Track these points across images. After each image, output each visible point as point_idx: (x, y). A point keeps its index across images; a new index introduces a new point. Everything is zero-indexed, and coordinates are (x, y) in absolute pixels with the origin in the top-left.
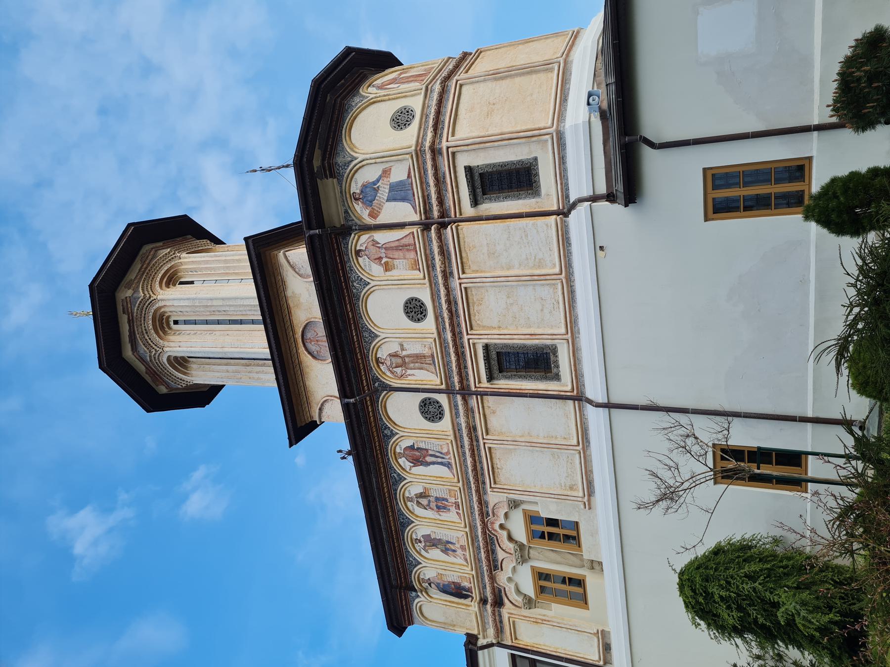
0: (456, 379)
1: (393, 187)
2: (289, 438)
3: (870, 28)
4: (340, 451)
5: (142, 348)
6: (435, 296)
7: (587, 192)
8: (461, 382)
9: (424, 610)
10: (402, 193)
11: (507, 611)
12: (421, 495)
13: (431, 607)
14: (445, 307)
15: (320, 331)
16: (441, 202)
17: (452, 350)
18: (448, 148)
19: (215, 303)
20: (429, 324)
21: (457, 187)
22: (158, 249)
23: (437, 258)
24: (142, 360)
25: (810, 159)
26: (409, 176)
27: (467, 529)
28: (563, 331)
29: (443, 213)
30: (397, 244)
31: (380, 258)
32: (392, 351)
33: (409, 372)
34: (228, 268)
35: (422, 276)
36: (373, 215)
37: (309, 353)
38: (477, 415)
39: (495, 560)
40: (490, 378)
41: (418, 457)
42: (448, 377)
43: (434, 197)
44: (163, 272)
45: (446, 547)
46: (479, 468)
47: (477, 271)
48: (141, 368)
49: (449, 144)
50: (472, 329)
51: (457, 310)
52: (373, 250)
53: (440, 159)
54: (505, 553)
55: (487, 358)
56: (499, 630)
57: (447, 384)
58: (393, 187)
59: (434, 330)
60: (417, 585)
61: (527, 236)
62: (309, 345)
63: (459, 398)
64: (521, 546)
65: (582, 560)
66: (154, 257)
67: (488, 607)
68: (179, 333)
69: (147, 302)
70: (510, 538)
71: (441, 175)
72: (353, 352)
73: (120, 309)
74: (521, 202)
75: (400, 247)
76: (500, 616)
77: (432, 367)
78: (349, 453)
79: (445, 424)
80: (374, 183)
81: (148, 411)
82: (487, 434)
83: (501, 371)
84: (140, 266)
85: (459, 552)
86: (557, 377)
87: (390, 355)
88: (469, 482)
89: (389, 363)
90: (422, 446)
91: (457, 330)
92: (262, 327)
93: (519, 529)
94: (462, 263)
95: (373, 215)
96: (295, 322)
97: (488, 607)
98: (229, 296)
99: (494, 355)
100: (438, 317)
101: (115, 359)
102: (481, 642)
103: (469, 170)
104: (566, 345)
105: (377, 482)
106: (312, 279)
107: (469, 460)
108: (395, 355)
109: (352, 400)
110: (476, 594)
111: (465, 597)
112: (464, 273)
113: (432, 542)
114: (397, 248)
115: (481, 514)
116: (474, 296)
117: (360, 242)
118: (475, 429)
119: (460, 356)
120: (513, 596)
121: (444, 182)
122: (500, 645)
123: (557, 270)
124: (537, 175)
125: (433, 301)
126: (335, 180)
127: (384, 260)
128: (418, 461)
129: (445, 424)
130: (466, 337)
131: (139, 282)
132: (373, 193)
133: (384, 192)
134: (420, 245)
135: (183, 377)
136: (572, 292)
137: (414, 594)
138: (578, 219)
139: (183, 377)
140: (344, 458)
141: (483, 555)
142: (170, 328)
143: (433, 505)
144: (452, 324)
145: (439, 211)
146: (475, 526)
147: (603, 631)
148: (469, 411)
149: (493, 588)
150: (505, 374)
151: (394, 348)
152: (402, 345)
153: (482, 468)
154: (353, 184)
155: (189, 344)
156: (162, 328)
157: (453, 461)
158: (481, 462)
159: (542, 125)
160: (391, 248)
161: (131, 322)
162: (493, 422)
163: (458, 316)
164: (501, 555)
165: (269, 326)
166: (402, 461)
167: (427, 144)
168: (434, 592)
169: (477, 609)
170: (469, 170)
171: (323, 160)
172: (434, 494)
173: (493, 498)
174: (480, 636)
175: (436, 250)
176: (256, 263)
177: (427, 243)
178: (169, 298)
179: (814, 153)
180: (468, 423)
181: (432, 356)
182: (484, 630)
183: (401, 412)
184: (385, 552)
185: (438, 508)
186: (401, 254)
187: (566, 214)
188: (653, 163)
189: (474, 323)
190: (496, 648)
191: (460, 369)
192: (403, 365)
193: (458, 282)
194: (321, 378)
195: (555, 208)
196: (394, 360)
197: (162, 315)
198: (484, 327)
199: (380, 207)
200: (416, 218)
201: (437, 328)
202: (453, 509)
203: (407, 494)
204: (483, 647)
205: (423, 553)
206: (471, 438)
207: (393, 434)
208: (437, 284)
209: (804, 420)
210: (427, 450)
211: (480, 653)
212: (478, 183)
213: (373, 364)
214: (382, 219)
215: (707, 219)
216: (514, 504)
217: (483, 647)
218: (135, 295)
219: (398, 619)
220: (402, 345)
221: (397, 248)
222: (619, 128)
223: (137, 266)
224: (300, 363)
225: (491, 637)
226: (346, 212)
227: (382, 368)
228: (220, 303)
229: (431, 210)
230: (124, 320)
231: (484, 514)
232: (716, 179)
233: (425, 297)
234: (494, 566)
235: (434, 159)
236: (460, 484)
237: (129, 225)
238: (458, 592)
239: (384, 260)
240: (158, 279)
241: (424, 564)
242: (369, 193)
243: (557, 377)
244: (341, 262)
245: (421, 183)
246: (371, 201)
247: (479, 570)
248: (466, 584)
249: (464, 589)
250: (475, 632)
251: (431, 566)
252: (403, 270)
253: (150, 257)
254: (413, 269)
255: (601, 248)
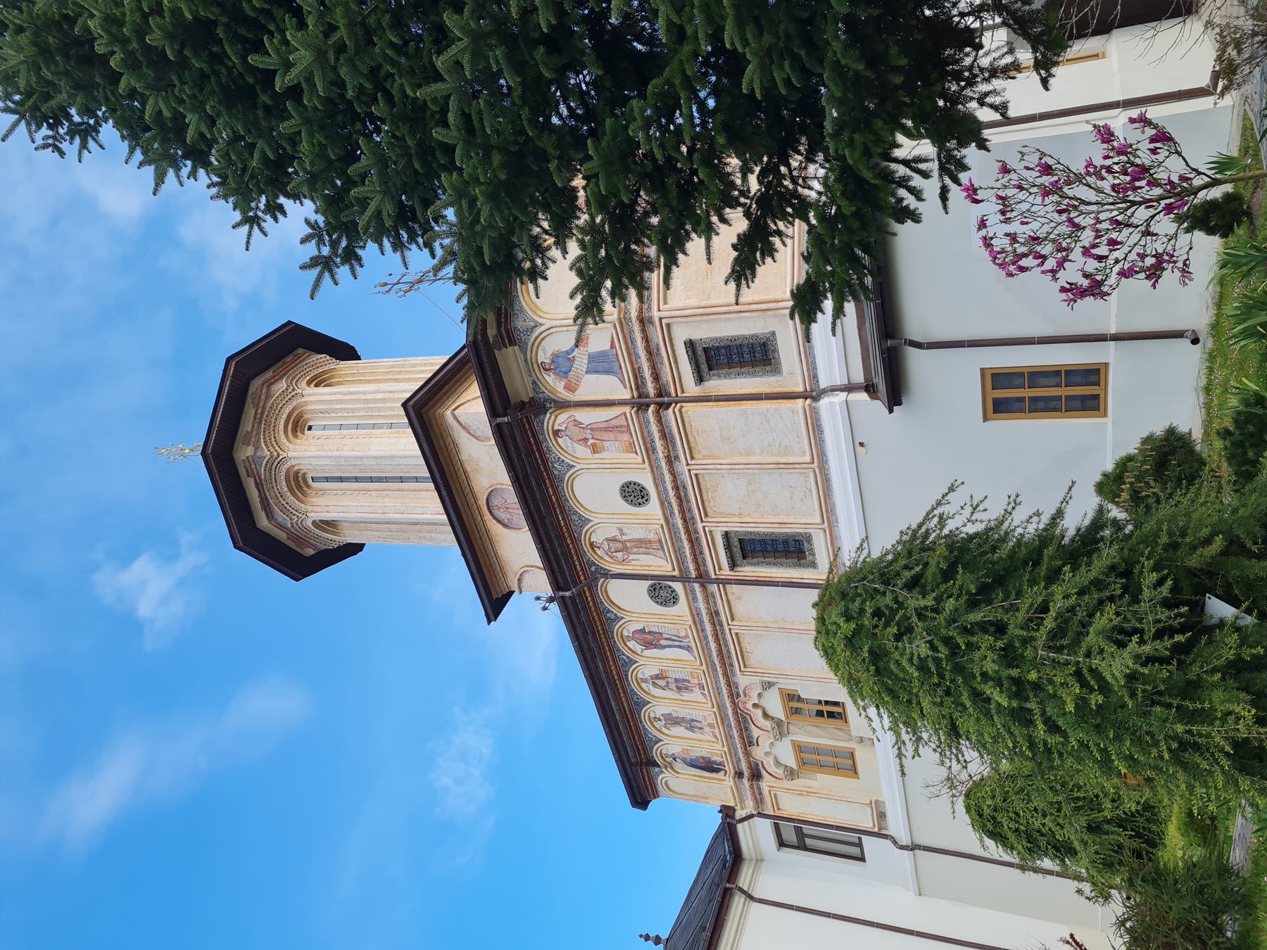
0: (691, 567)
1: (592, 358)
2: (487, 615)
3: (1159, 429)
4: (538, 598)
5: (280, 516)
6: (658, 481)
7: (840, 380)
8: (698, 568)
9: (670, 784)
10: (605, 365)
11: (766, 783)
12: (657, 677)
13: (677, 783)
14: (671, 493)
15: (510, 496)
16: (656, 377)
17: (684, 537)
18: (661, 319)
19: (366, 462)
20: (653, 508)
21: (676, 362)
22: (270, 383)
23: (659, 444)
24: (282, 527)
25: (1106, 365)
26: (612, 346)
27: (715, 709)
28: (818, 520)
29: (661, 392)
30: (605, 425)
31: (586, 440)
32: (610, 535)
33: (632, 557)
34: (370, 408)
35: (640, 460)
36: (570, 388)
37: (499, 521)
38: (719, 601)
39: (750, 737)
40: (733, 565)
41: (651, 640)
42: (681, 562)
43: (647, 373)
44: (285, 416)
45: (691, 725)
46: (724, 651)
47: (709, 457)
48: (281, 535)
49: (662, 314)
50: (706, 515)
51: (686, 495)
52: (575, 430)
53: (650, 329)
54: (761, 731)
55: (728, 547)
56: (759, 800)
57: (680, 570)
58: (592, 358)
59: (660, 516)
60: (659, 761)
61: (768, 421)
62: (496, 512)
63: (696, 586)
64: (779, 723)
65: (850, 735)
66: (268, 396)
67: (745, 781)
68: (324, 492)
69: (275, 462)
70: (766, 715)
71: (653, 347)
72: (561, 537)
73: (242, 472)
74: (757, 380)
75: (609, 428)
76: (759, 788)
77: (660, 553)
78: (551, 600)
79: (682, 607)
80: (568, 353)
81: (297, 580)
82: (733, 619)
83: (744, 557)
84: (253, 411)
85: (707, 729)
86: (813, 565)
87: (607, 539)
88: (713, 665)
89: (606, 548)
90: (654, 629)
91: (688, 515)
92: (432, 485)
93: (777, 709)
94: (690, 449)
95: (570, 388)
96: (476, 488)
97: (745, 781)
98: (383, 454)
99: (735, 542)
100: (664, 503)
101: (250, 536)
102: (740, 814)
103: (691, 345)
104: (822, 535)
105: (604, 666)
106: (493, 442)
107: (713, 646)
108: (614, 540)
109: (568, 594)
110: (729, 768)
111: (718, 770)
112: (692, 458)
113: (673, 721)
114: (606, 430)
115: (731, 695)
116: (706, 483)
117: (558, 422)
118: (717, 613)
119: (694, 541)
120: (771, 767)
121: (659, 354)
122: (761, 815)
123: (808, 458)
124: (775, 351)
125: (656, 486)
126: (516, 348)
127: (591, 442)
128: (649, 645)
129: (682, 607)
130: (700, 525)
131: (258, 434)
132: (567, 363)
133: (581, 362)
134: (635, 427)
135: (330, 537)
136: (827, 480)
137: (657, 769)
138: (830, 406)
139: (330, 537)
140: (545, 609)
141: (736, 734)
142: (309, 487)
143: (673, 686)
144: (682, 511)
145: (655, 388)
146: (724, 705)
147: (876, 802)
148: (708, 597)
149: (749, 763)
150: (750, 560)
151: (613, 532)
152: (621, 530)
153: (729, 651)
154: (540, 353)
155: (339, 509)
156: (300, 488)
157: (693, 645)
158: (726, 646)
159: (779, 297)
160: (600, 429)
161: (259, 485)
162: (738, 608)
163: (688, 501)
164: (755, 732)
165: (444, 493)
166: (631, 644)
167: (634, 314)
168: (679, 766)
169: (732, 783)
170: (691, 345)
171: (499, 326)
172: (672, 675)
173: (742, 681)
174: (738, 808)
175: (656, 435)
176: (420, 431)
177: (644, 425)
178: (303, 452)
179: (1111, 360)
180: (709, 609)
181: (660, 541)
182: (742, 801)
183: (628, 601)
184: (620, 734)
185: (679, 688)
186: (611, 435)
187: (816, 399)
188: (918, 364)
189: (708, 510)
190: (756, 819)
191: (695, 556)
192: (625, 549)
193: (686, 468)
194: (517, 548)
195: (800, 389)
196: (611, 544)
197: (297, 473)
198: (722, 514)
199: (579, 379)
200: (626, 395)
201: (664, 514)
202: (696, 689)
203: (640, 676)
204: (742, 820)
205: (664, 730)
206: (713, 624)
207: (618, 619)
208: (659, 467)
209: (1117, 338)
210: (661, 634)
211: (739, 826)
212: (702, 359)
213: (587, 548)
214: (580, 396)
215: (986, 419)
216: (768, 685)
217: (742, 820)
218: (259, 453)
219: (641, 795)
220: (621, 530)
221: (606, 430)
222: (879, 330)
223: (249, 413)
224: (487, 532)
225: (750, 807)
226: (534, 383)
227: (598, 551)
228: (373, 462)
229: (644, 384)
230: (250, 485)
231: (734, 696)
232: (997, 378)
233: (647, 481)
234: (748, 742)
235: (644, 331)
236: (704, 667)
237: (229, 360)
238: (709, 766)
239: (591, 442)
240: (282, 427)
241: (578, 467)
242: (562, 364)
243: (813, 565)
244: (536, 442)
245: (629, 355)
246: (566, 373)
247: (731, 746)
248: (717, 759)
249: (715, 763)
250: (732, 804)
251: (672, 742)
252: (614, 452)
253: (263, 397)
254: (628, 451)
255: (861, 444)
